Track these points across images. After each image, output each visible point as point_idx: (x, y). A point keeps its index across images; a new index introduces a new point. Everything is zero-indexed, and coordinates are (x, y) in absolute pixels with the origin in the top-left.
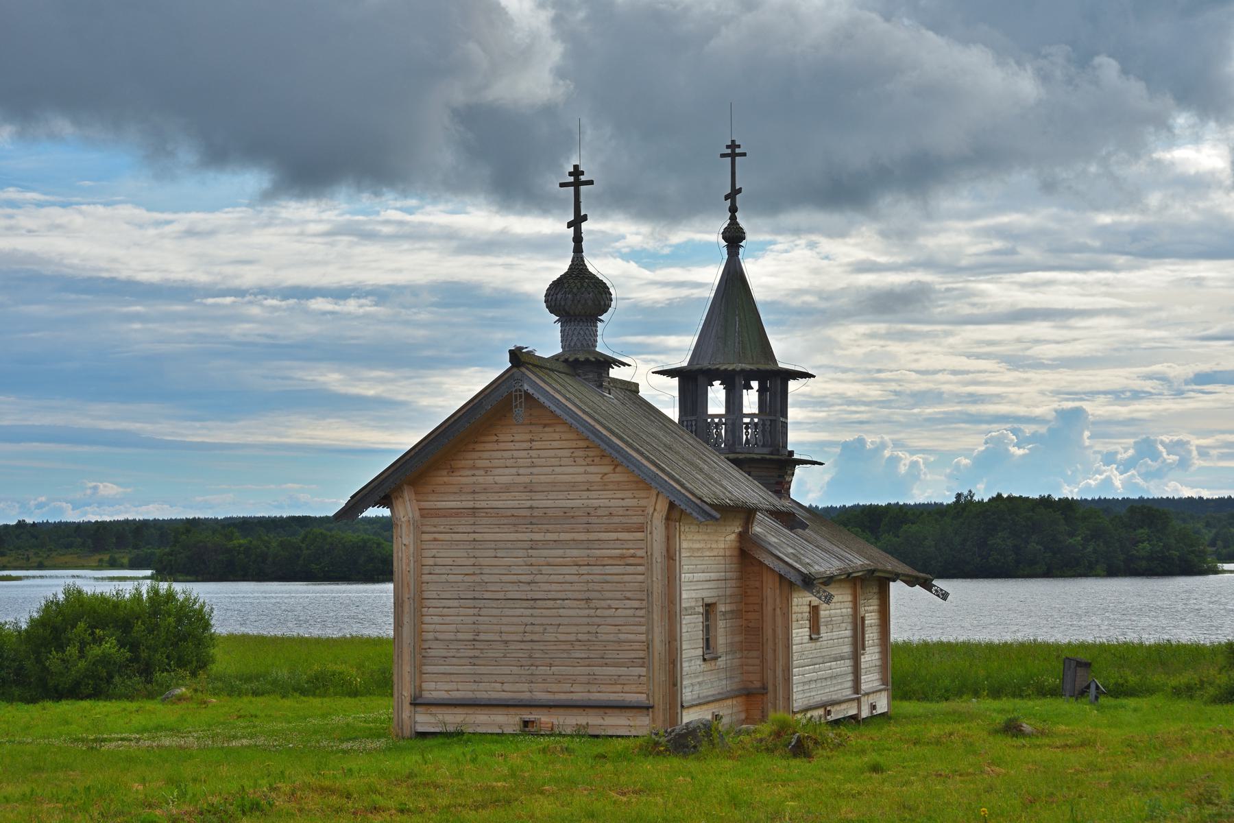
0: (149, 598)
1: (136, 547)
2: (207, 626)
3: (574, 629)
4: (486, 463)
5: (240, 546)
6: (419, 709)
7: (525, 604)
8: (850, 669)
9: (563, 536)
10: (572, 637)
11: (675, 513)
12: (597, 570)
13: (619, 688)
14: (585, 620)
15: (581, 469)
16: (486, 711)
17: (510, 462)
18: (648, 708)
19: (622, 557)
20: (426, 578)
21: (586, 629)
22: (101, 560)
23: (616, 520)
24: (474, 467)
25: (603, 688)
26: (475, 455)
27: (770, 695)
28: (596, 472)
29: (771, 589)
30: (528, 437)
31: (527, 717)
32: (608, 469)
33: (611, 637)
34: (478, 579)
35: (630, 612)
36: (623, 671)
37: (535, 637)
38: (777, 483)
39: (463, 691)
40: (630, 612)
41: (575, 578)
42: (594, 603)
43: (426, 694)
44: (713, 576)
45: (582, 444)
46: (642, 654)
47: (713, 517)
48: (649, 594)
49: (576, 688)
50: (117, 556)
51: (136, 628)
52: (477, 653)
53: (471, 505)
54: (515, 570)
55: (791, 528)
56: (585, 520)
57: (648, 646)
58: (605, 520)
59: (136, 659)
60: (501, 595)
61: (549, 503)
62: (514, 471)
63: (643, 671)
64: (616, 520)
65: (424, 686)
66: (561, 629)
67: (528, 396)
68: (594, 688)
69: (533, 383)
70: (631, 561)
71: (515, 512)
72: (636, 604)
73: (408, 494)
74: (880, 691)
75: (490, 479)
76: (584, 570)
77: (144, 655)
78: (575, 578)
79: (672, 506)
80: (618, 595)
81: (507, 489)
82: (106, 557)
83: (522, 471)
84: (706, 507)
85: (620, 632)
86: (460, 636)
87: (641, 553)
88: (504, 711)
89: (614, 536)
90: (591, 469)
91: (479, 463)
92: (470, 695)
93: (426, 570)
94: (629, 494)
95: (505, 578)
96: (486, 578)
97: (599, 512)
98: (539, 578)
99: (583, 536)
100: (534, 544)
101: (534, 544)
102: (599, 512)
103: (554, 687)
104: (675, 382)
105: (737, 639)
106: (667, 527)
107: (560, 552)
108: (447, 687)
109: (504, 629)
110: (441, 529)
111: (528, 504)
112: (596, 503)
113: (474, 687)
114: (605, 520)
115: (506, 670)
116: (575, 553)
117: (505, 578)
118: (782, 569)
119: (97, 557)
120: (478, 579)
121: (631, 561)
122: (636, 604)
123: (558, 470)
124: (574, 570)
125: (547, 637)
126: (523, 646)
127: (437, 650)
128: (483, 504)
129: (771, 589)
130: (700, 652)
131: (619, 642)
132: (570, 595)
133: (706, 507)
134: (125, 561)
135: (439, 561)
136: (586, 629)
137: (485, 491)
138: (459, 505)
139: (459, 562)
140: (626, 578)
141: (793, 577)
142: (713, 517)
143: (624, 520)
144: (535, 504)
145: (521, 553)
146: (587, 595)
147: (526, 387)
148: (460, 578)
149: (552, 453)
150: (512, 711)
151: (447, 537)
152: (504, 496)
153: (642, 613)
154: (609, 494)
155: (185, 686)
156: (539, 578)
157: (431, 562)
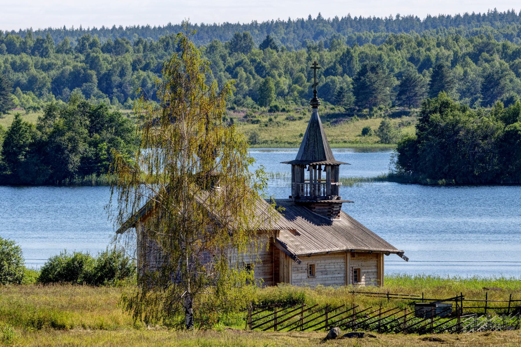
38: (329, 211)
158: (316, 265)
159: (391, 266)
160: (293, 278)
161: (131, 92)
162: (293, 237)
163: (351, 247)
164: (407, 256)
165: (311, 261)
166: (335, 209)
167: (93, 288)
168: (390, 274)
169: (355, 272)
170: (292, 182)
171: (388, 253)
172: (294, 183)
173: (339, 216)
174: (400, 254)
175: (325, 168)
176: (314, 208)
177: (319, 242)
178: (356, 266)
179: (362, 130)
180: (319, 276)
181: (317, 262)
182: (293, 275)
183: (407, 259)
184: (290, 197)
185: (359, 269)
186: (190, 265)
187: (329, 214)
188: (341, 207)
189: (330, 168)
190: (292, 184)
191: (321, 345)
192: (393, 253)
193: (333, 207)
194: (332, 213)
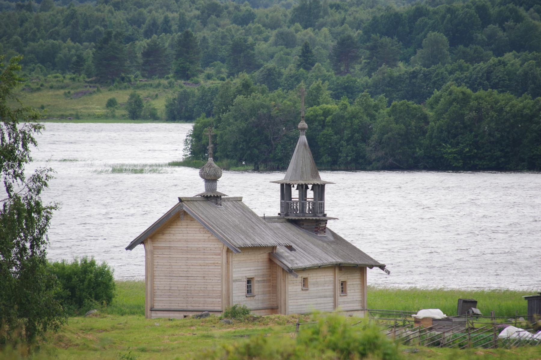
0: (82, 264)
1: (184, 74)
2: (111, 279)
3: (200, 286)
4: (173, 232)
5: (326, 113)
6: (153, 312)
7: (186, 278)
8: (332, 301)
9: (197, 256)
10: (199, 289)
11: (231, 250)
12: (207, 267)
13: (213, 305)
14: (203, 284)
15: (202, 235)
16: (173, 312)
17: (181, 232)
18: (221, 312)
19: (214, 263)
20: (155, 269)
21: (203, 286)
22: (111, 103)
23: (212, 251)
24: (170, 233)
25: (208, 305)
26: (170, 229)
27: (279, 309)
28: (207, 235)
29: (280, 273)
30: (186, 224)
31: (185, 314)
32: (210, 235)
33: (211, 289)
34: (171, 269)
35: (217, 281)
36: (214, 300)
37: (188, 289)
38: (316, 228)
39: (167, 307)
40: (217, 281)
41: (200, 270)
42: (206, 278)
43: (155, 307)
44: (262, 268)
45: (202, 227)
46: (220, 294)
47: (238, 251)
48: (222, 275)
49: (200, 305)
50: (142, 94)
51: (74, 280)
52: (171, 294)
53: (169, 245)
54: (182, 267)
55: (291, 251)
56: (203, 251)
57: (222, 291)
58: (209, 251)
59: (73, 295)
60: (178, 275)
61: (193, 246)
62: (182, 235)
63: (220, 300)
64: (212, 251)
65: (155, 304)
66: (196, 286)
67: (185, 212)
68: (206, 305)
69: (186, 207)
70: (217, 265)
71: (183, 248)
72: (218, 278)
73: (149, 241)
74: (229, 303)
75: (175, 237)
76: (203, 267)
77: (78, 293)
78: (200, 270)
79: (228, 249)
80: (213, 275)
81: (180, 241)
82: (123, 96)
83: (184, 235)
84: (237, 249)
85: (213, 287)
86: (166, 288)
87: (220, 262)
88: (178, 312)
89: (212, 256)
90: (205, 235)
91: (171, 232)
92: (168, 307)
93: (155, 266)
94: (216, 243)
95: (179, 270)
96: (173, 269)
97: (208, 249)
98: (189, 270)
99: (202, 257)
100: (188, 259)
101: (188, 259)
102: (208, 249)
103: (194, 305)
104: (280, 185)
105: (268, 289)
106: (227, 254)
107: (195, 262)
108: (162, 304)
109: (179, 286)
110: (160, 253)
111: (186, 246)
112: (206, 246)
113: (170, 304)
114: (209, 251)
115: (179, 299)
116: (200, 262)
117: (179, 270)
118: (283, 266)
119: (105, 95)
120: (171, 269)
121: (217, 265)
122: (218, 278)
123: (195, 235)
124: (200, 267)
125: (192, 289)
126: (184, 291)
127: (158, 293)
128: (173, 245)
129: (280, 273)
130: (245, 294)
131: (213, 290)
132: (199, 275)
133: (237, 249)
134: (160, 105)
135: (159, 264)
136: (203, 286)
137: (173, 241)
138: (165, 245)
139: (166, 264)
140: (215, 270)
141: (286, 269)
142: (238, 251)
143: (215, 251)
144: (188, 246)
145: (184, 261)
146: (204, 275)
147: (184, 209)
148: (166, 269)
149: (193, 229)
150: (181, 312)
151: (161, 256)
152: (179, 243)
153: (220, 281)
154: (210, 243)
155: (96, 309)
156: (189, 270)
157: (156, 264)
158: (309, 278)
159: (373, 276)
160: (289, 290)
161: (179, 34)
162: (288, 253)
163: (340, 260)
164: (389, 269)
165: (304, 275)
166: (321, 226)
167: (104, 266)
168: (370, 284)
169: (342, 284)
170: (281, 200)
171: (371, 267)
172: (283, 201)
173: (325, 232)
174: (382, 267)
175: (312, 187)
176: (303, 225)
177: (311, 257)
178: (343, 279)
179: (200, 177)
180: (312, 288)
181: (310, 276)
182: (290, 288)
183: (388, 273)
184: (279, 214)
185: (345, 282)
186: (15, 142)
187: (316, 230)
188: (326, 223)
189: (317, 187)
190: (281, 202)
191: (324, 356)
192: (376, 266)
193: (320, 224)
194: (319, 229)
